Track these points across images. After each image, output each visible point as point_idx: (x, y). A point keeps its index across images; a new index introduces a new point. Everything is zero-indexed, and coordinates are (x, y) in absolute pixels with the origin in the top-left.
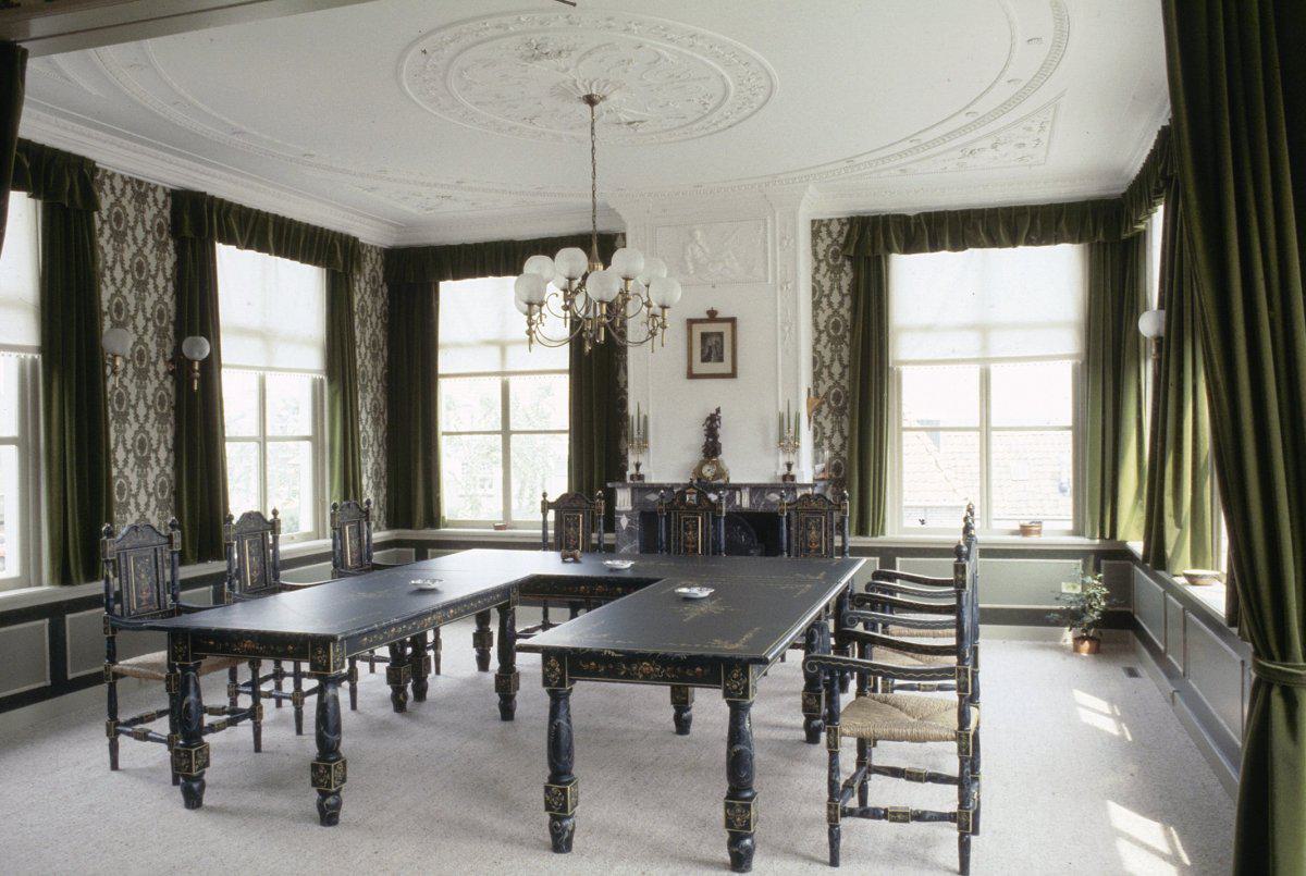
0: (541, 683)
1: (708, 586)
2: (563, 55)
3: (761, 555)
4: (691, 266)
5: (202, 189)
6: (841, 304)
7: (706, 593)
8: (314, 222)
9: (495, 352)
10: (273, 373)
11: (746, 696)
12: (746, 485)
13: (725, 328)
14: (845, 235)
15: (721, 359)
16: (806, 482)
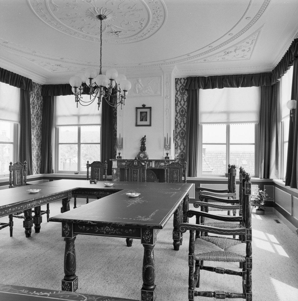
0: (61, 235)
1: (138, 192)
3: (158, 182)
4: (137, 91)
6: (184, 104)
7: (137, 195)
9: (76, 118)
11: (152, 243)
12: (154, 160)
13: (148, 110)
15: (146, 120)
16: (173, 159)
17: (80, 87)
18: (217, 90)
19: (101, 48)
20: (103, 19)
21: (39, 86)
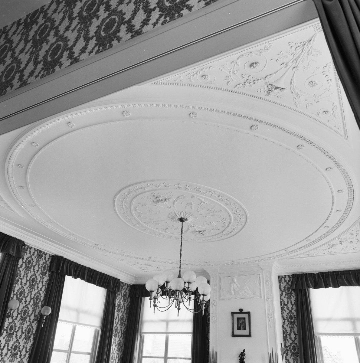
2: (167, 200)
4: (233, 291)
5: (62, 255)
6: (292, 308)
9: (164, 324)
10: (79, 325)
13: (246, 316)
14: (291, 281)
15: (245, 329)
17: (158, 290)
18: (331, 290)
19: (181, 249)
20: (184, 221)
21: (128, 286)
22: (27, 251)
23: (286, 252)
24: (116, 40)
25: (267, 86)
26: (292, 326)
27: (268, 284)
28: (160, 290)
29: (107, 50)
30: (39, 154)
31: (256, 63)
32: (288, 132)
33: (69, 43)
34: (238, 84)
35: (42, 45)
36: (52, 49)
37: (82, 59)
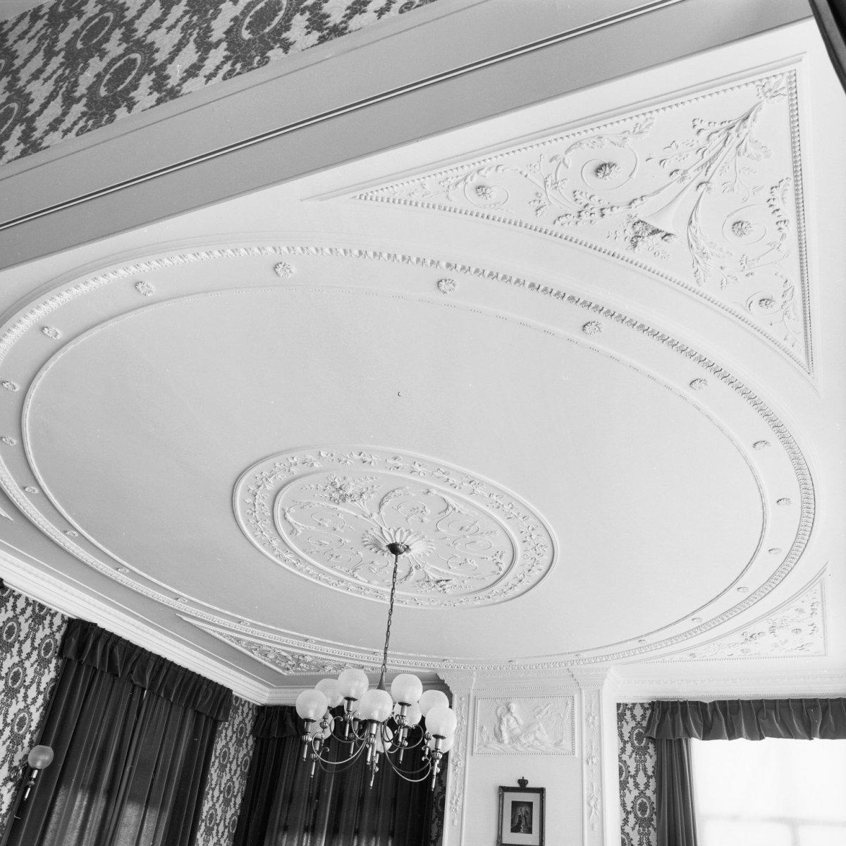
6: (647, 786)
8: (192, 668)
13: (533, 798)
14: (647, 719)
15: (529, 831)
18: (742, 745)
19: (389, 620)
20: (401, 553)
22: (7, 604)
23: (640, 645)
24: (280, 47)
25: (631, 224)
26: (644, 830)
27: (593, 723)
28: (330, 718)
29: (253, 71)
30: (59, 356)
31: (611, 165)
32: (673, 344)
33: (156, 56)
34: (564, 214)
35: (87, 61)
36: (112, 70)
37: (187, 91)
